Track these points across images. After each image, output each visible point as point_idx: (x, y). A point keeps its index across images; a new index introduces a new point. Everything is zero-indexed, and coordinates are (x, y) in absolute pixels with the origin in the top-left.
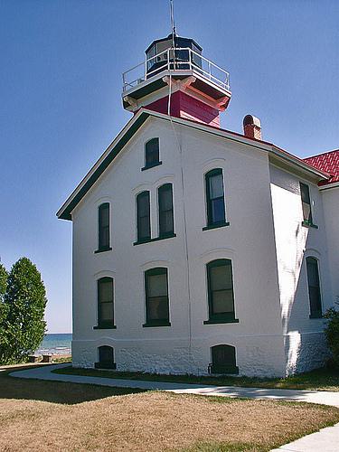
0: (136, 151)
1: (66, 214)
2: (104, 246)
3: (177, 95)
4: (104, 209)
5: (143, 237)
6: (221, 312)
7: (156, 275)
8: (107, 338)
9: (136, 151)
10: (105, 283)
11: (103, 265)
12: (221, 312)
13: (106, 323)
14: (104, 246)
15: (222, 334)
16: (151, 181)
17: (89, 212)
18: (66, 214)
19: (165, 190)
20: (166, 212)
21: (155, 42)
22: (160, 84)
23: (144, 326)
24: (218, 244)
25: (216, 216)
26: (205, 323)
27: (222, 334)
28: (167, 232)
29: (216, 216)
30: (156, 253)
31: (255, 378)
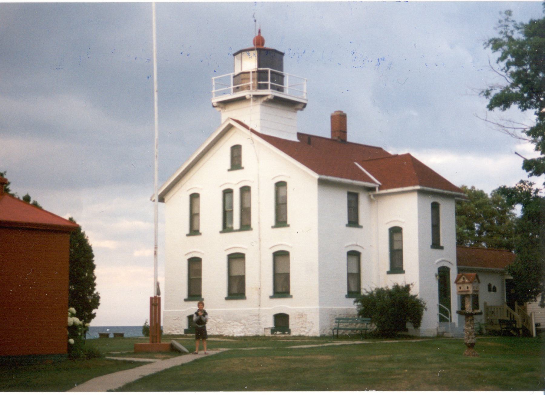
4: (194, 197)
5: (226, 228)
19: (245, 190)
20: (246, 212)
28: (246, 226)
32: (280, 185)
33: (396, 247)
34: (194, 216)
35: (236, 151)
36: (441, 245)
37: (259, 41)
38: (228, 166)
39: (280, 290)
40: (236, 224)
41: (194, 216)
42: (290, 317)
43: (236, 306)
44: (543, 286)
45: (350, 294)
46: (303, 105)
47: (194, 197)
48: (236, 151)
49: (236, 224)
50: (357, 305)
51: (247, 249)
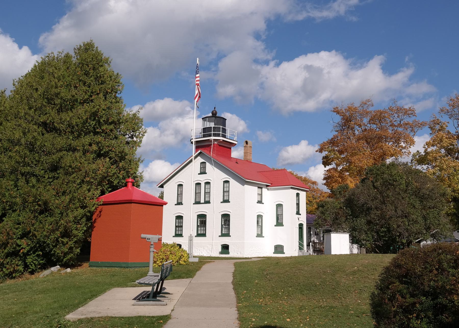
2: (179, 203)
16: (203, 179)
20: (207, 193)
34: (180, 194)
40: (202, 201)
41: (180, 194)
47: (180, 186)
49: (202, 201)
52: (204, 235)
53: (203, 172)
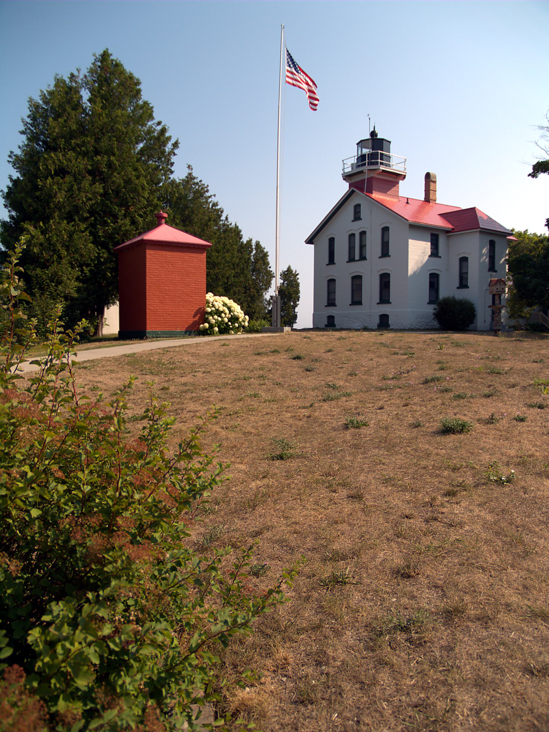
0: (349, 211)
1: (310, 241)
2: (331, 261)
3: (370, 180)
4: (332, 241)
5: (351, 259)
6: (384, 299)
7: (357, 280)
8: (332, 311)
9: (349, 211)
10: (331, 282)
11: (332, 272)
12: (384, 299)
13: (331, 303)
14: (331, 261)
15: (385, 309)
16: (357, 227)
17: (324, 241)
18: (310, 241)
19: (363, 234)
20: (362, 247)
21: (361, 141)
22: (362, 172)
23: (458, 288)
24: (385, 265)
25: (385, 253)
26: (378, 304)
27: (385, 309)
28: (363, 258)
29: (385, 253)
30: (358, 268)
31: (88, 360)
32: (385, 230)
33: (464, 271)
35: (357, 208)
36: (391, 301)
37: (373, 134)
38: (352, 218)
39: (356, 299)
40: (357, 257)
42: (390, 317)
43: (357, 309)
44: (66, 298)
45: (430, 302)
46: (403, 176)
47: (332, 241)
48: (357, 208)
49: (357, 257)
50: (18, 178)
51: (362, 273)
52: (359, 303)
53: (357, 217)
